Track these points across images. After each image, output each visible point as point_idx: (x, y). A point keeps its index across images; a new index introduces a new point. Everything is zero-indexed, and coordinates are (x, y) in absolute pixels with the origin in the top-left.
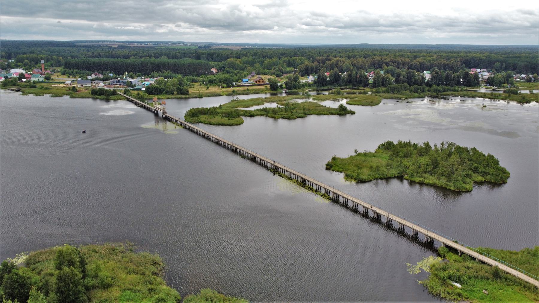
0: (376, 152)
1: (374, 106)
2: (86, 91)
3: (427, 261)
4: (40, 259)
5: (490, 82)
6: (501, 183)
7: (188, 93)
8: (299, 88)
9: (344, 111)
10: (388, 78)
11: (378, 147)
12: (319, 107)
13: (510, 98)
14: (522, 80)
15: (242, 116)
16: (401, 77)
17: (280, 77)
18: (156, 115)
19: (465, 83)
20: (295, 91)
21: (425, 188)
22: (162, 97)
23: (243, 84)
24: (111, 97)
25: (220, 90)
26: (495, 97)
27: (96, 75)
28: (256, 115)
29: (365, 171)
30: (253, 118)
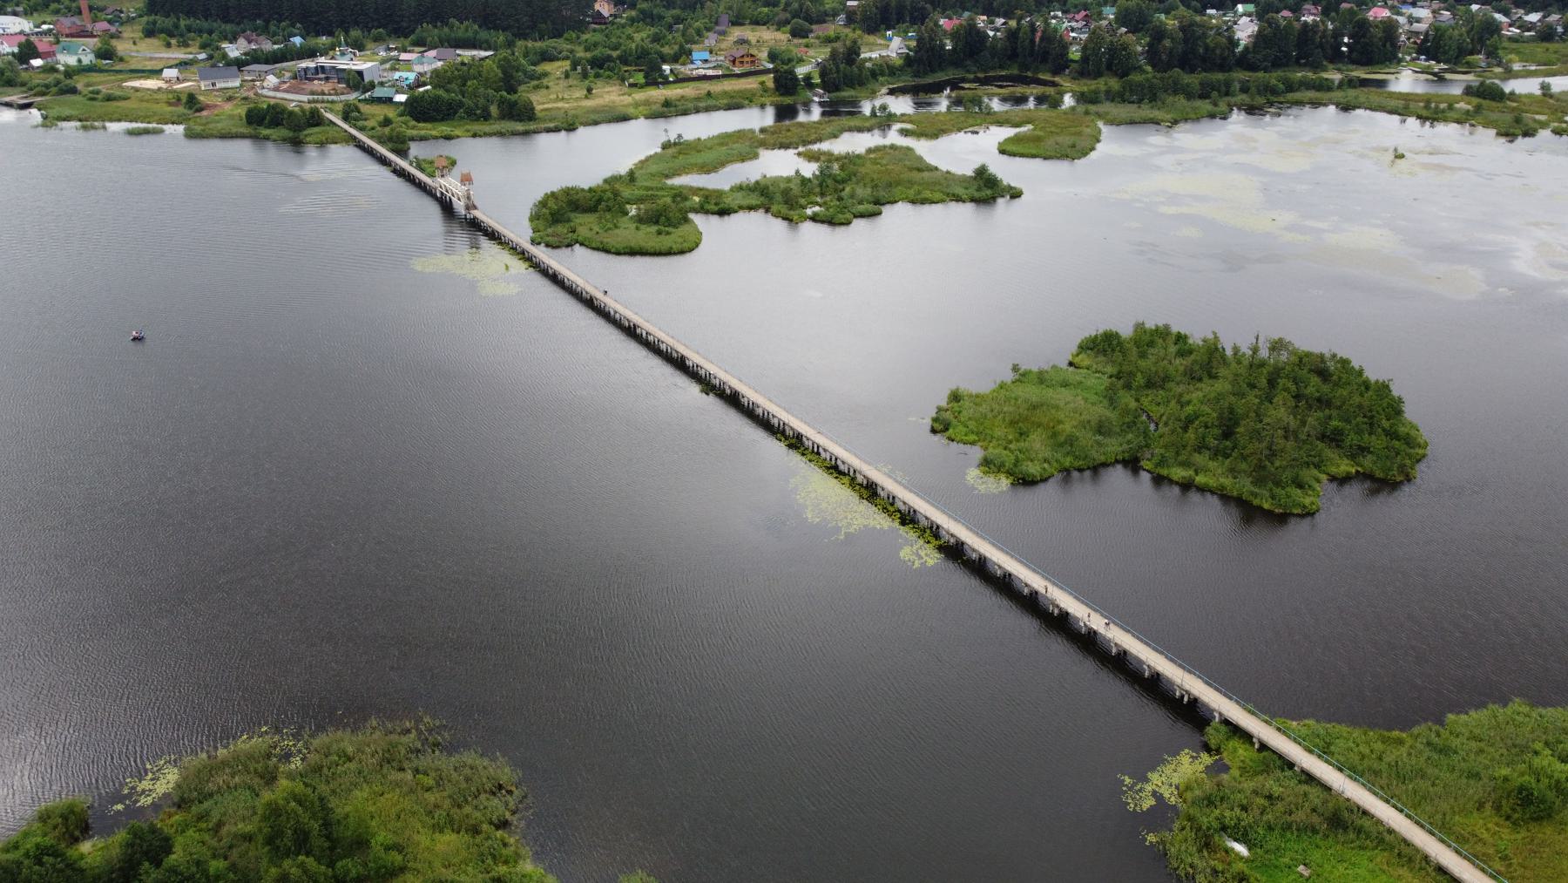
0: (1071, 364)
1: (1079, 158)
2: (228, 107)
3: (1173, 766)
4: (211, 787)
5: (1433, 47)
6: (1399, 479)
7: (534, 113)
8: (862, 84)
9: (992, 188)
10: (1125, 49)
11: (1076, 348)
12: (919, 170)
13: (1480, 119)
14: (1526, 34)
15: (696, 211)
16: (1167, 43)
17: (803, 37)
18: (446, 207)
19: (1354, 55)
20: (849, 97)
21: (1195, 497)
22: (457, 132)
23: (692, 70)
24: (305, 132)
25: (627, 100)
26: (1436, 113)
27: (250, 42)
28: (736, 208)
29: (1037, 445)
30: (726, 218)
